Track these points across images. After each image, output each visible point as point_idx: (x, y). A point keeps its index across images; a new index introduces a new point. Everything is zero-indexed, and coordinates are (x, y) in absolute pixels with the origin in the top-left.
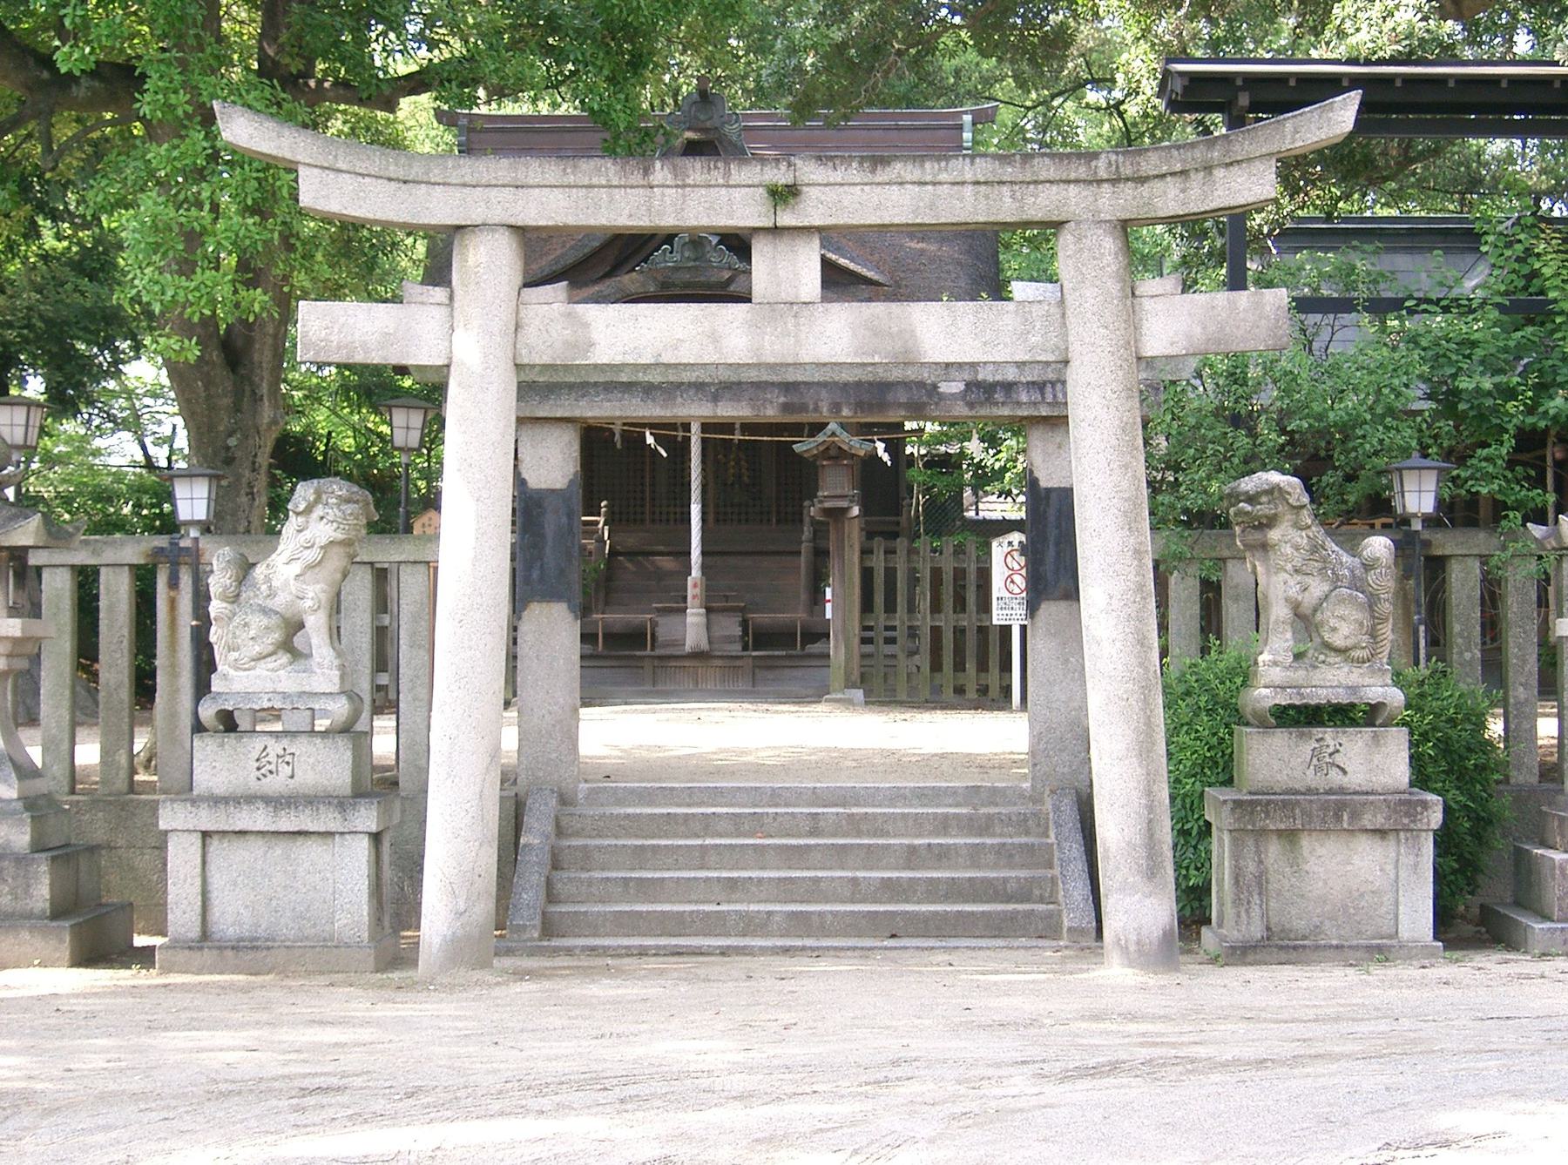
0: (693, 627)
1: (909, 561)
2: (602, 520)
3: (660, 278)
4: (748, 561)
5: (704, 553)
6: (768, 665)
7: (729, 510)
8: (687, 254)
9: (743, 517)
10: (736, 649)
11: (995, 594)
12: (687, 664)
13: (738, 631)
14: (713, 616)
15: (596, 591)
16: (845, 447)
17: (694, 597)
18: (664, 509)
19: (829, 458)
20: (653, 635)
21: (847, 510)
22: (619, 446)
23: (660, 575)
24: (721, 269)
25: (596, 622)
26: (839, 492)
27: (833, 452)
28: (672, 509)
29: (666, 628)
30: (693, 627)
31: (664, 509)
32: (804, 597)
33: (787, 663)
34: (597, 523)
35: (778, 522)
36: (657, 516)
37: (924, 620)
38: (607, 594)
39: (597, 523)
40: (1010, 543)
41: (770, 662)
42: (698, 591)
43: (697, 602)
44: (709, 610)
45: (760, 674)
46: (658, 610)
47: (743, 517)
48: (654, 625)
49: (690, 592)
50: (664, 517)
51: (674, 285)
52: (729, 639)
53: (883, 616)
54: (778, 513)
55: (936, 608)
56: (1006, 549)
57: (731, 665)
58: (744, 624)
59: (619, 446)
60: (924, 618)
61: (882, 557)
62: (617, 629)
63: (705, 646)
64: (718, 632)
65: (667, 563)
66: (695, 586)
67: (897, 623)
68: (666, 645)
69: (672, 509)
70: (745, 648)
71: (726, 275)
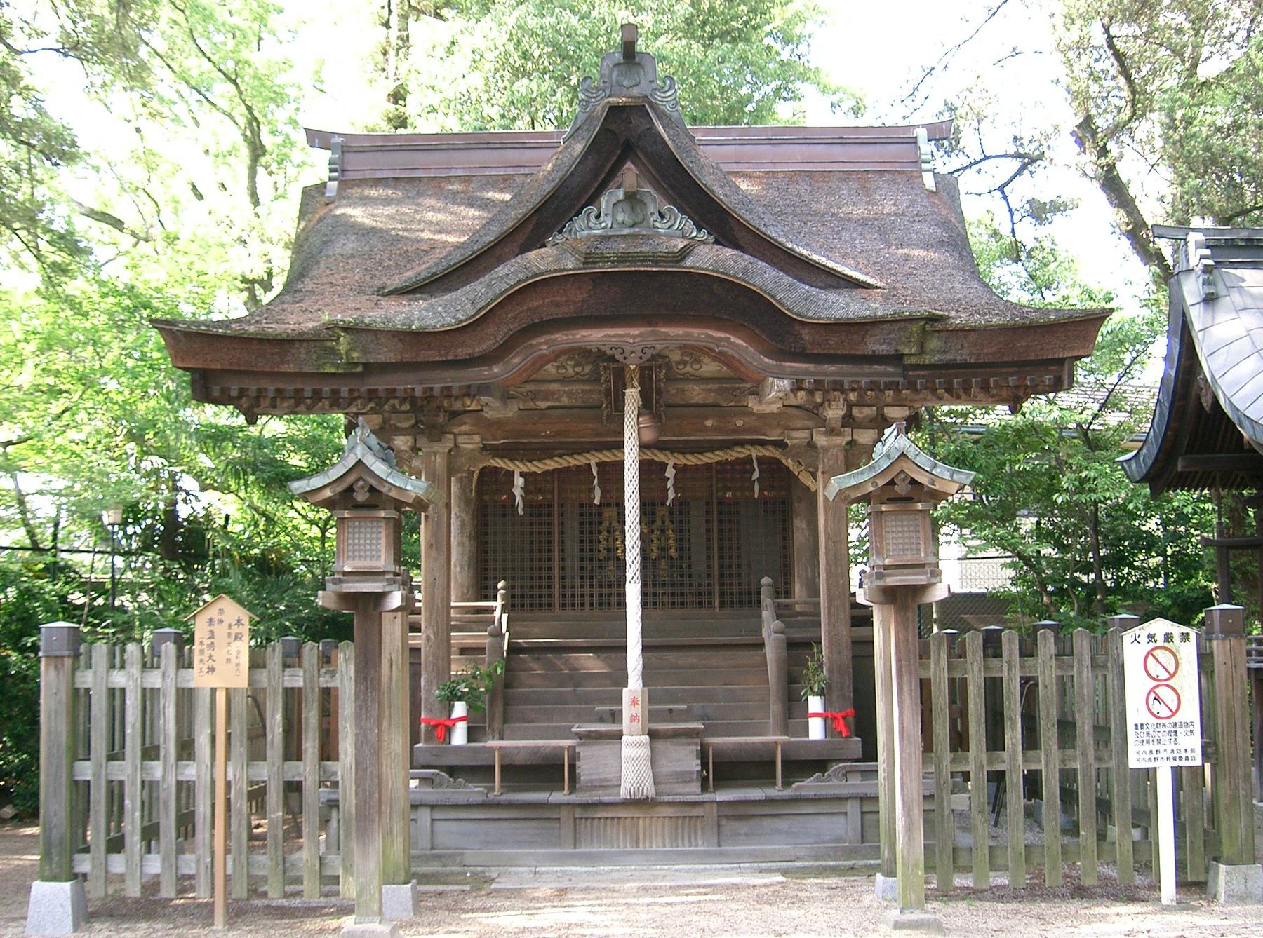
0: (631, 763)
1: (986, 668)
2: (498, 604)
3: (583, 248)
4: (691, 658)
5: (645, 648)
6: (739, 812)
7: (659, 591)
8: (620, 218)
9: (678, 599)
10: (692, 791)
11: (1131, 720)
12: (622, 813)
13: (695, 765)
14: (660, 745)
15: (492, 703)
16: (923, 479)
17: (633, 718)
18: (578, 591)
19: (891, 500)
20: (573, 767)
21: (380, 597)
22: (520, 512)
23: (576, 679)
24: (670, 237)
25: (491, 749)
26: (908, 558)
27: (901, 489)
28: (587, 590)
29: (591, 763)
30: (631, 763)
31: (578, 591)
32: (775, 707)
33: (766, 811)
34: (492, 610)
35: (722, 604)
36: (569, 600)
37: (1014, 760)
38: (506, 704)
39: (492, 610)
40: (1151, 637)
41: (741, 810)
42: (638, 710)
43: (637, 726)
44: (653, 735)
45: (728, 826)
46: (580, 736)
47: (678, 599)
48: (574, 758)
49: (627, 710)
50: (577, 600)
51: (603, 258)
52: (683, 778)
53: (948, 756)
54: (722, 594)
55: (1031, 740)
56: (1146, 646)
57: (686, 817)
58: (703, 756)
59: (520, 512)
60: (1013, 758)
61: (944, 663)
62: (520, 760)
63: (649, 790)
64: (666, 767)
65: (590, 663)
66: (634, 702)
67: (971, 767)
68: (592, 787)
69: (587, 590)
70: (705, 788)
71: (681, 244)
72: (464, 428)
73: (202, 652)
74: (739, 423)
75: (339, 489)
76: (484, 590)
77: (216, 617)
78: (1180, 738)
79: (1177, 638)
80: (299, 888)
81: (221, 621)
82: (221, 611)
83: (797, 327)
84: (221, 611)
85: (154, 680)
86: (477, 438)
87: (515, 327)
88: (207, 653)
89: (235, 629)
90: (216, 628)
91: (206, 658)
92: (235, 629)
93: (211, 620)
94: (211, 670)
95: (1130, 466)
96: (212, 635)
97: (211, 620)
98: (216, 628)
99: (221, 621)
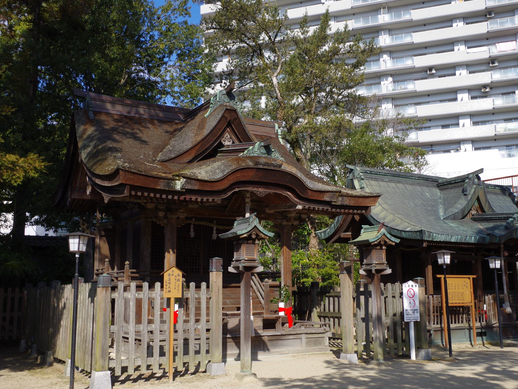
40: (409, 285)
72: (181, 211)
73: (166, 285)
74: (263, 216)
75: (248, 234)
76: (113, 269)
77: (171, 273)
78: (415, 313)
79: (414, 286)
80: (457, 322)
81: (173, 275)
82: (173, 271)
83: (308, 190)
84: (173, 271)
85: (141, 295)
86: (185, 214)
87: (232, 182)
88: (168, 286)
89: (177, 278)
90: (171, 277)
91: (167, 287)
92: (177, 278)
93: (169, 274)
94: (169, 291)
95: (321, 234)
96: (170, 279)
97: (169, 274)
98: (171, 277)
99: (173, 275)
